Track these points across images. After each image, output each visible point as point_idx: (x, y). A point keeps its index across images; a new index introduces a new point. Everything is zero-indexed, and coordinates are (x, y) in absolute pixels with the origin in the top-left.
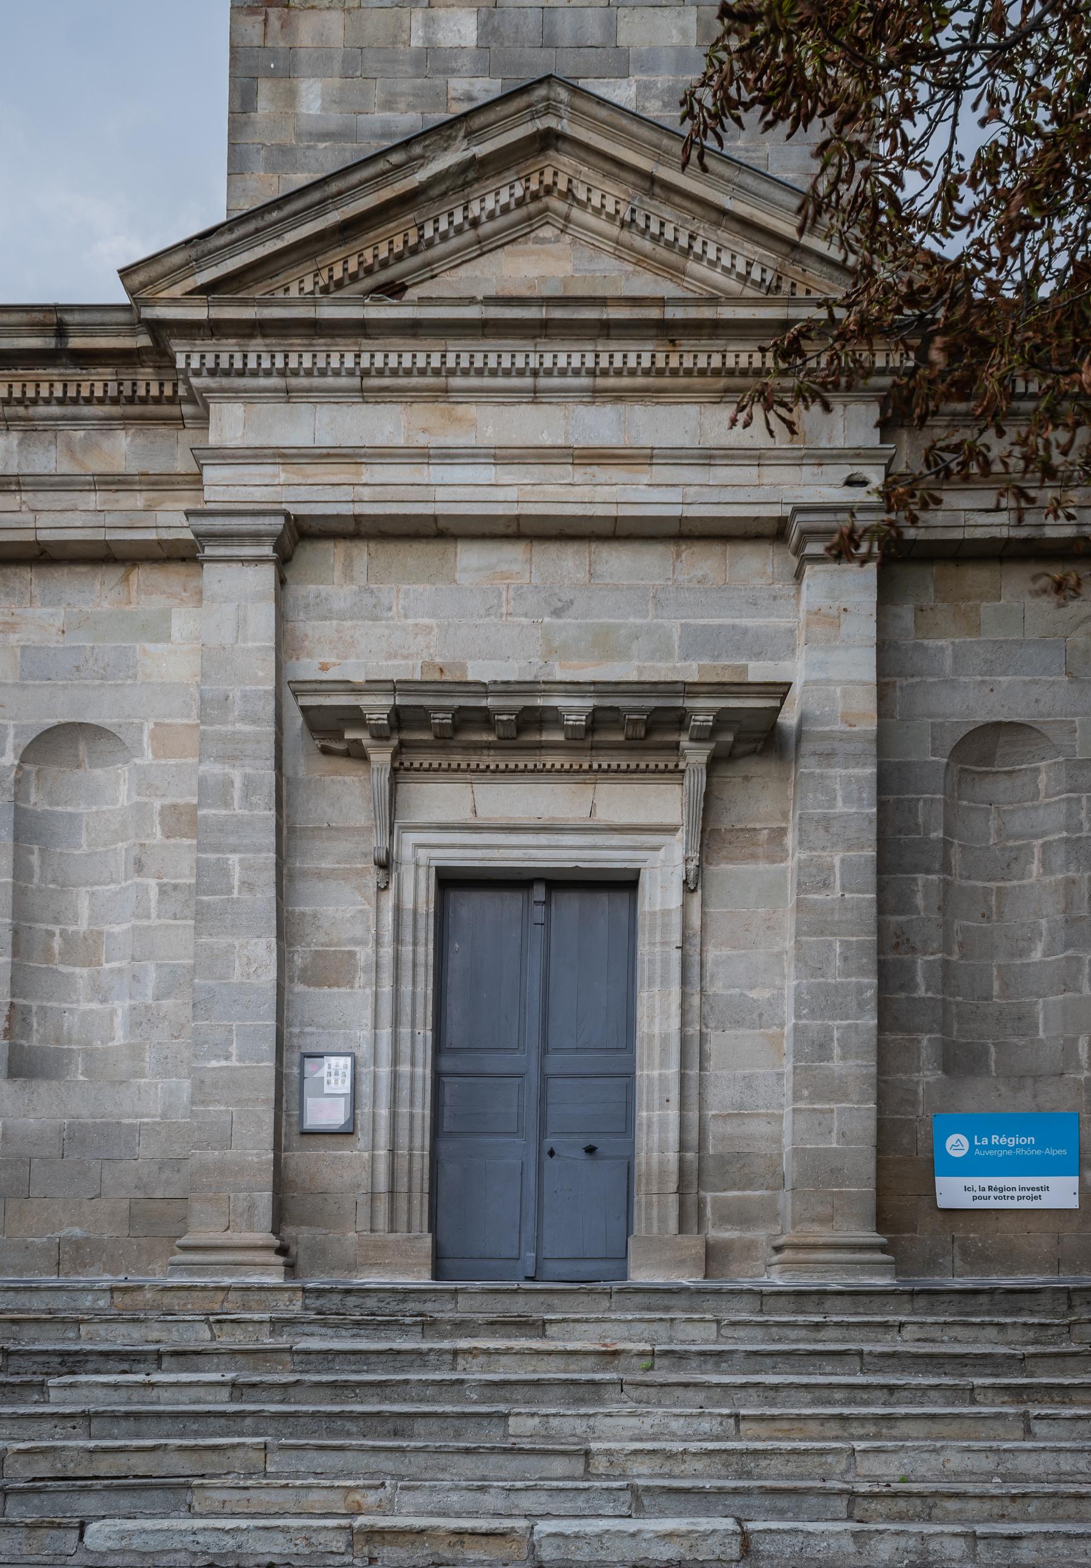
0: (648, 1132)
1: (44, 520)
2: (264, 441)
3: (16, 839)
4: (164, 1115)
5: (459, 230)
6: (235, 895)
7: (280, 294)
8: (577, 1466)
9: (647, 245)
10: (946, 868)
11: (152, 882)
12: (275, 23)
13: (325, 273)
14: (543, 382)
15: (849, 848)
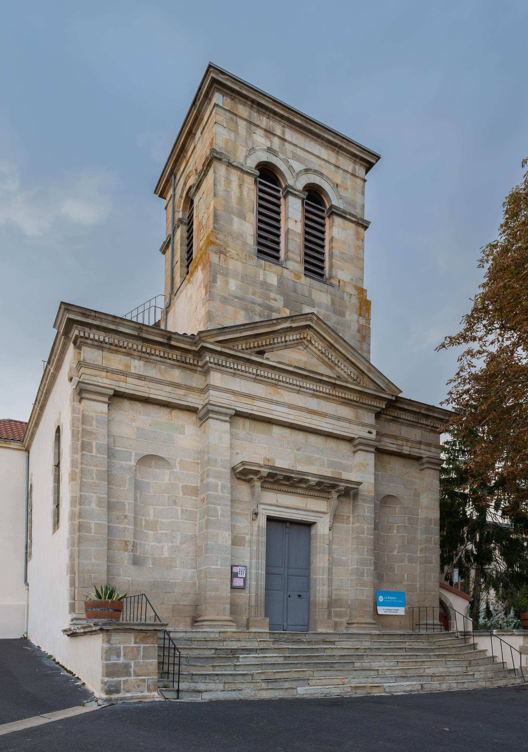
1: (152, 391)
2: (227, 386)
4: (183, 580)
5: (282, 342)
7: (236, 348)
8: (376, 673)
12: (222, 259)
14: (302, 389)
15: (368, 524)
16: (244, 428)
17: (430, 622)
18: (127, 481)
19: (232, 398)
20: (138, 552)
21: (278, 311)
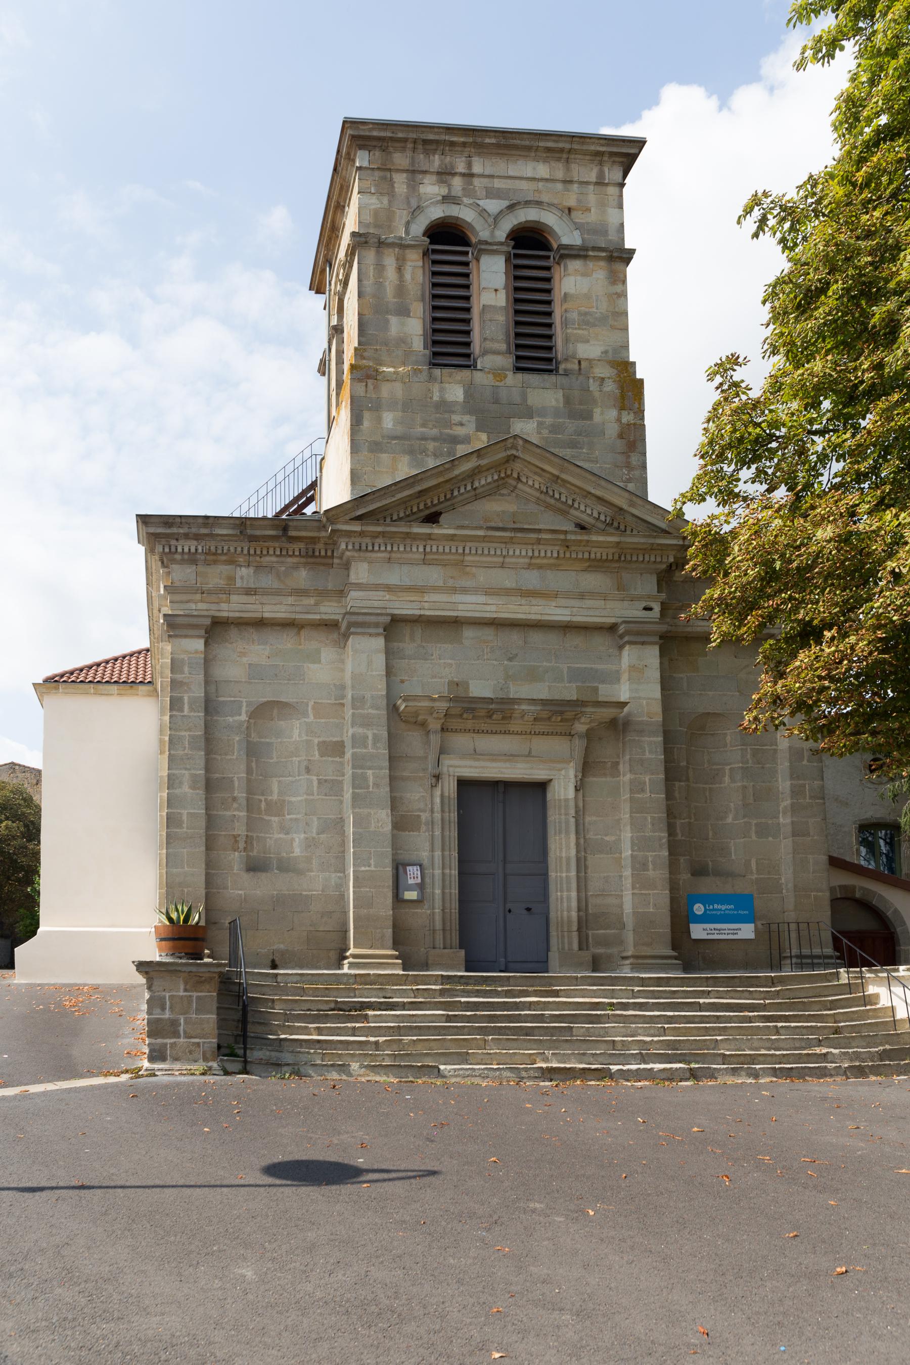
0: (561, 902)
2: (378, 580)
3: (247, 756)
4: (323, 891)
6: (371, 789)
9: (552, 501)
10: (688, 780)
11: (315, 778)
12: (371, 387)
13: (409, 509)
15: (652, 774)
16: (412, 639)
17: (817, 951)
18: (236, 745)
19: (387, 597)
20: (255, 851)
21: (466, 440)
